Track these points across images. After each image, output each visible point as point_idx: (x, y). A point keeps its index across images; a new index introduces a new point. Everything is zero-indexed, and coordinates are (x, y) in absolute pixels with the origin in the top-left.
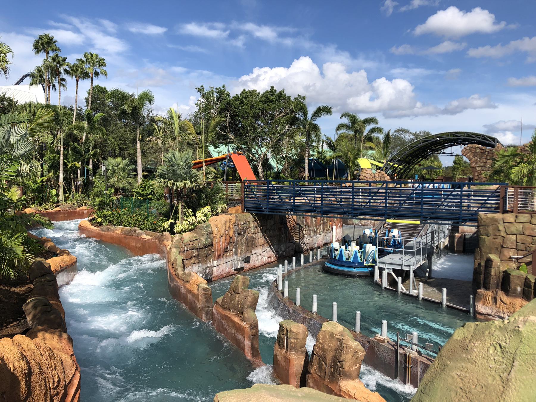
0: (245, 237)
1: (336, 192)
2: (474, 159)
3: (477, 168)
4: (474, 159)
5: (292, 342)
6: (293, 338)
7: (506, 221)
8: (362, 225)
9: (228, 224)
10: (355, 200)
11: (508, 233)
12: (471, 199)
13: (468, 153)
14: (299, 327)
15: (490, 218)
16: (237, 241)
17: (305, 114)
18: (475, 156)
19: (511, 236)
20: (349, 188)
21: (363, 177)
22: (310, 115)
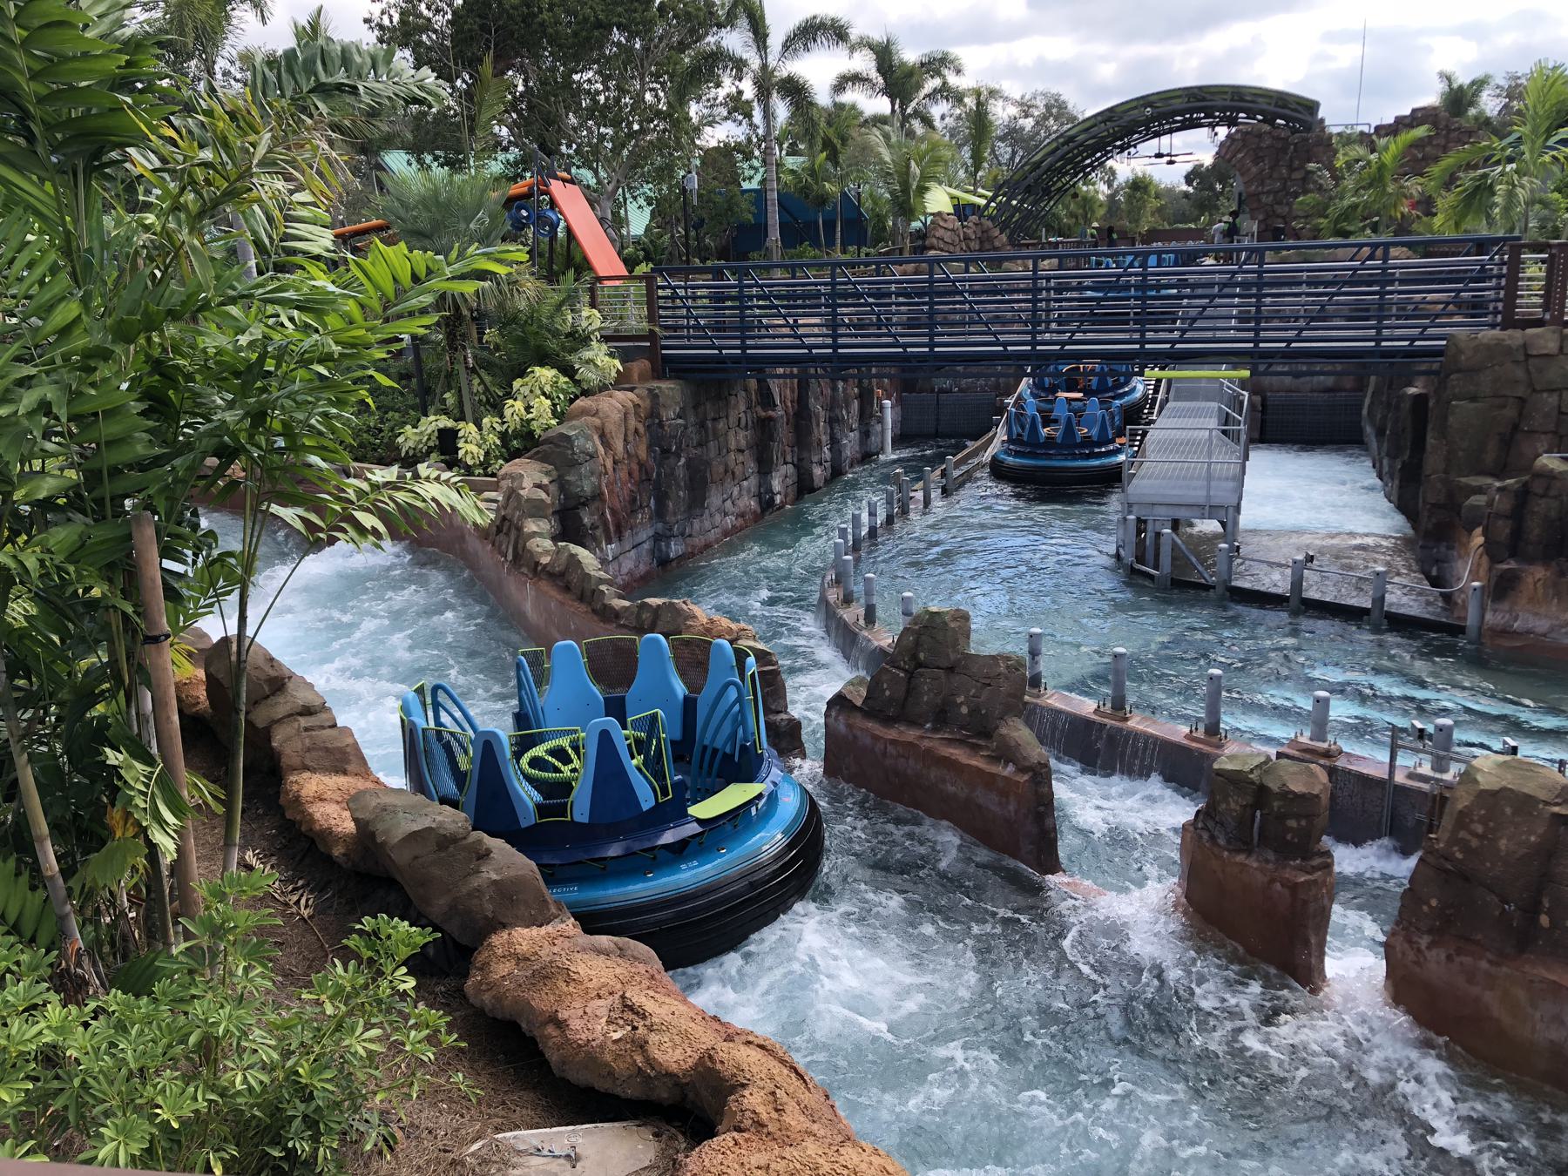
0: (683, 460)
1: (889, 295)
2: (1254, 170)
3: (1264, 199)
4: (1254, 170)
5: (1291, 829)
6: (1298, 817)
7: (1535, 353)
8: (961, 390)
9: (633, 422)
10: (939, 318)
11: (1538, 387)
12: (890, 305)
13: (1239, 151)
14: (1312, 774)
15: (1488, 347)
16: (659, 475)
17: (760, 34)
18: (1257, 160)
19: (1545, 395)
20: (816, 284)
21: (934, 241)
22: (775, 41)
